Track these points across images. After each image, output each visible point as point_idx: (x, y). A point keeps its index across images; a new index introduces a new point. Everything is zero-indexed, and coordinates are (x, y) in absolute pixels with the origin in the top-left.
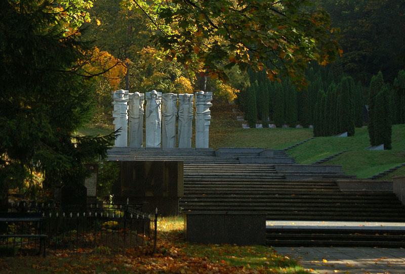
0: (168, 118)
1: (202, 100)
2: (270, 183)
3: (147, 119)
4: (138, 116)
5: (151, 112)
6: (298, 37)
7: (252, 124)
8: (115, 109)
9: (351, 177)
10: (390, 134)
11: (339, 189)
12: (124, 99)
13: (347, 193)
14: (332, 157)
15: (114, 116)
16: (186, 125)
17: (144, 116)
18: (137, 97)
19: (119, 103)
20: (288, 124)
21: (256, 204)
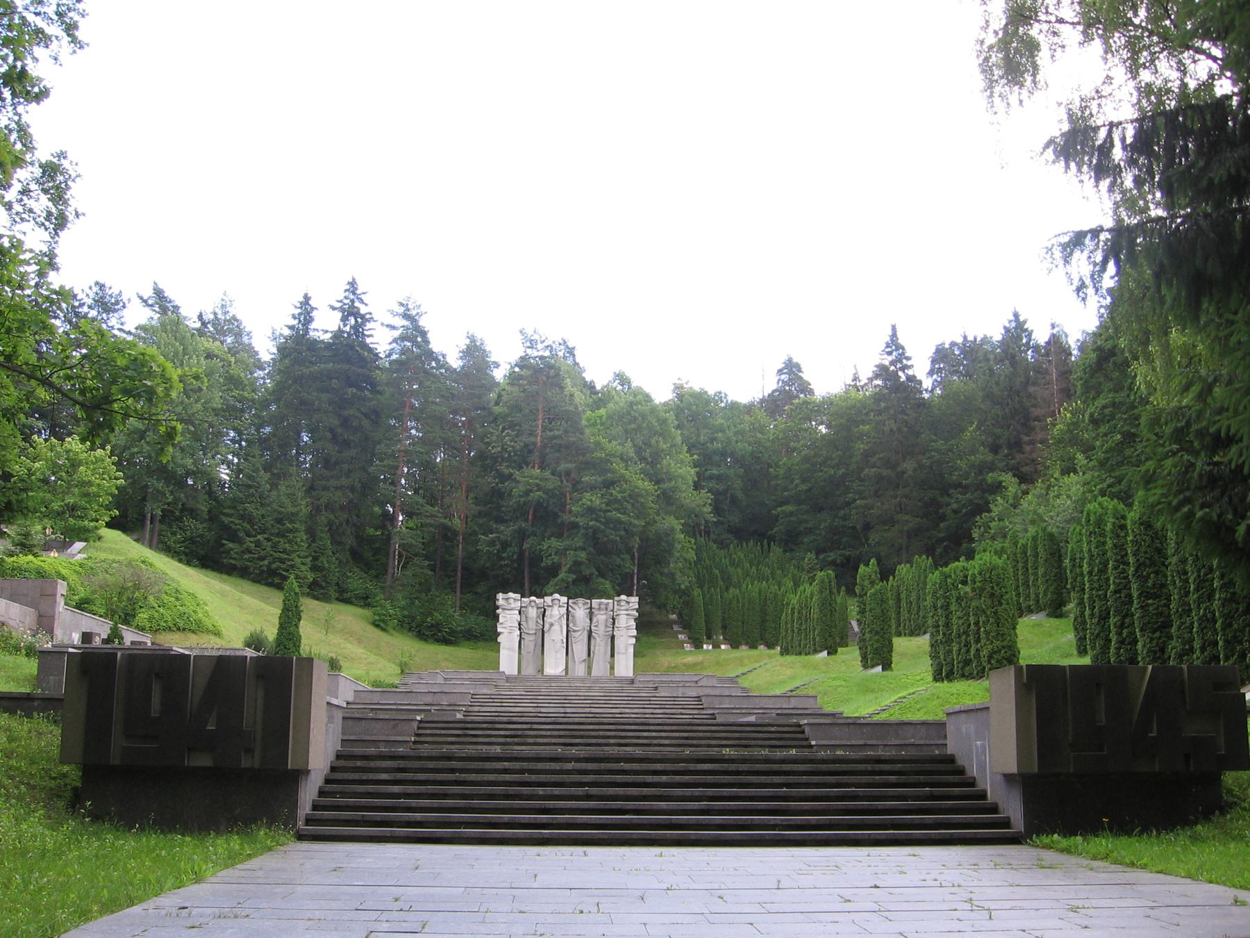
0: (576, 634)
1: (623, 608)
2: (660, 728)
3: (546, 635)
4: (534, 632)
5: (552, 625)
6: (1179, 853)
7: (698, 645)
8: (501, 620)
9: (833, 715)
10: (891, 651)
11: (807, 739)
12: (513, 606)
13: (674, 756)
14: (798, 688)
15: (499, 630)
16: (602, 644)
17: (543, 631)
18: (533, 604)
19: (506, 611)
20: (747, 644)
21: (411, 789)
